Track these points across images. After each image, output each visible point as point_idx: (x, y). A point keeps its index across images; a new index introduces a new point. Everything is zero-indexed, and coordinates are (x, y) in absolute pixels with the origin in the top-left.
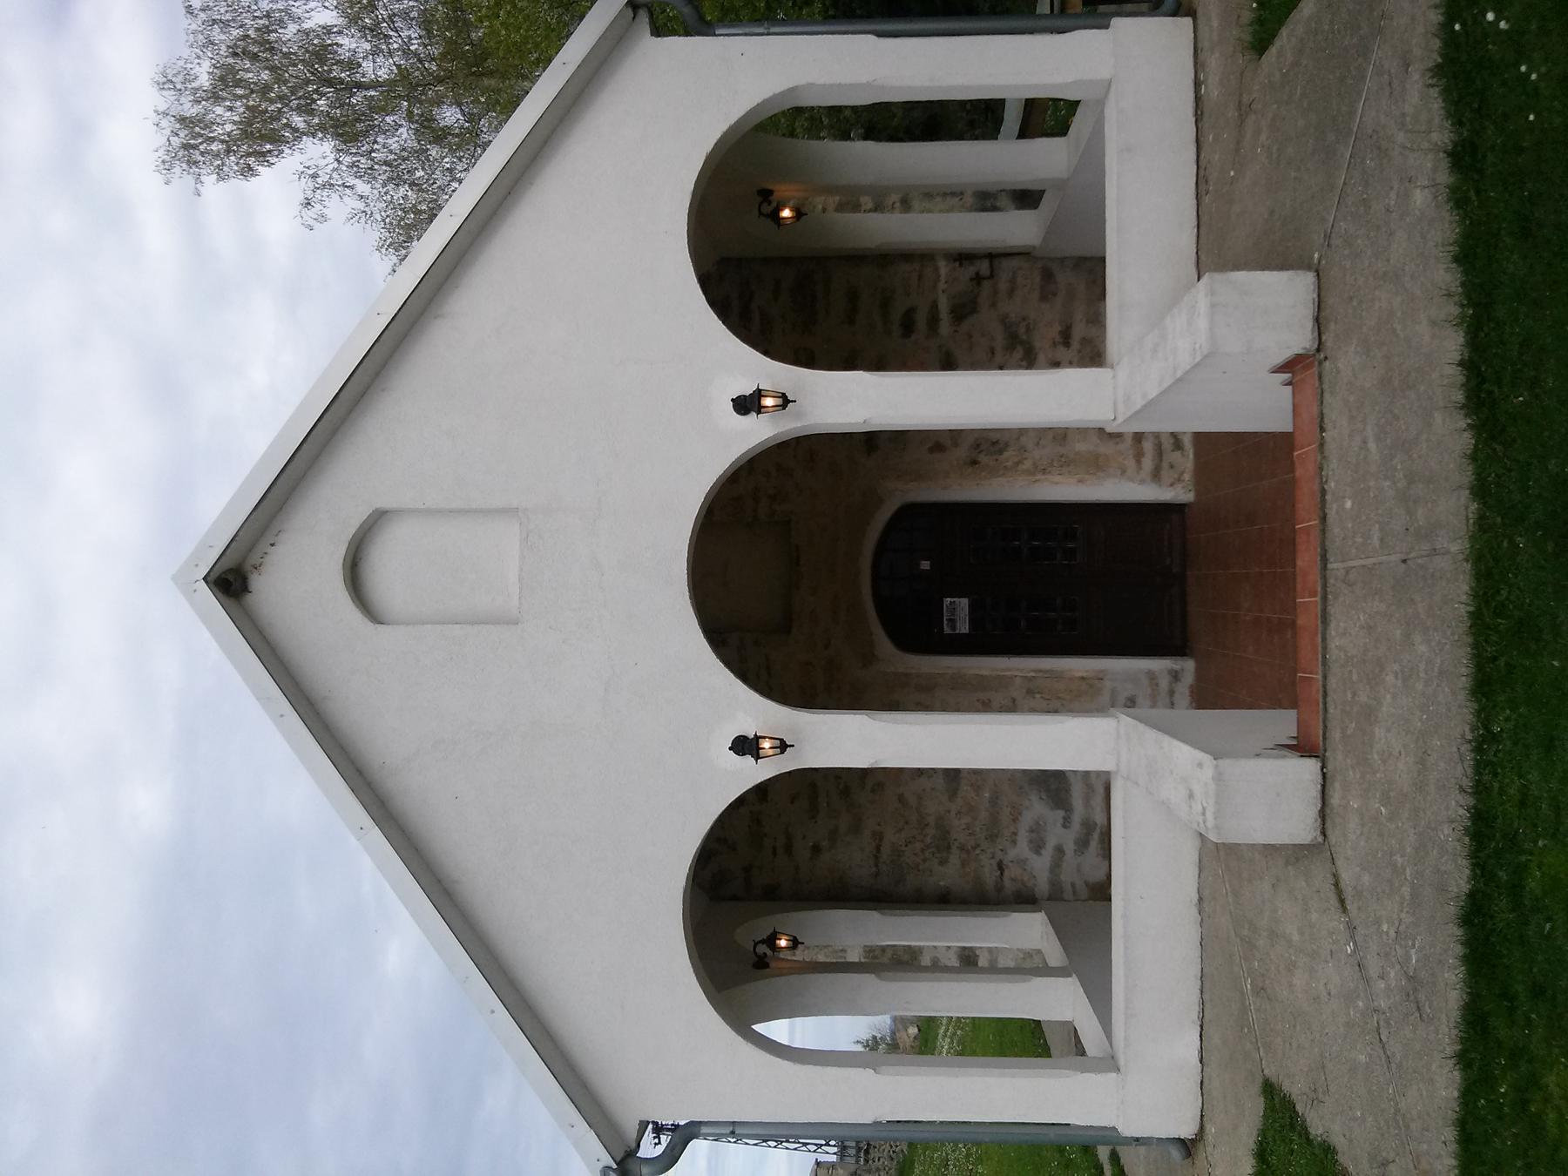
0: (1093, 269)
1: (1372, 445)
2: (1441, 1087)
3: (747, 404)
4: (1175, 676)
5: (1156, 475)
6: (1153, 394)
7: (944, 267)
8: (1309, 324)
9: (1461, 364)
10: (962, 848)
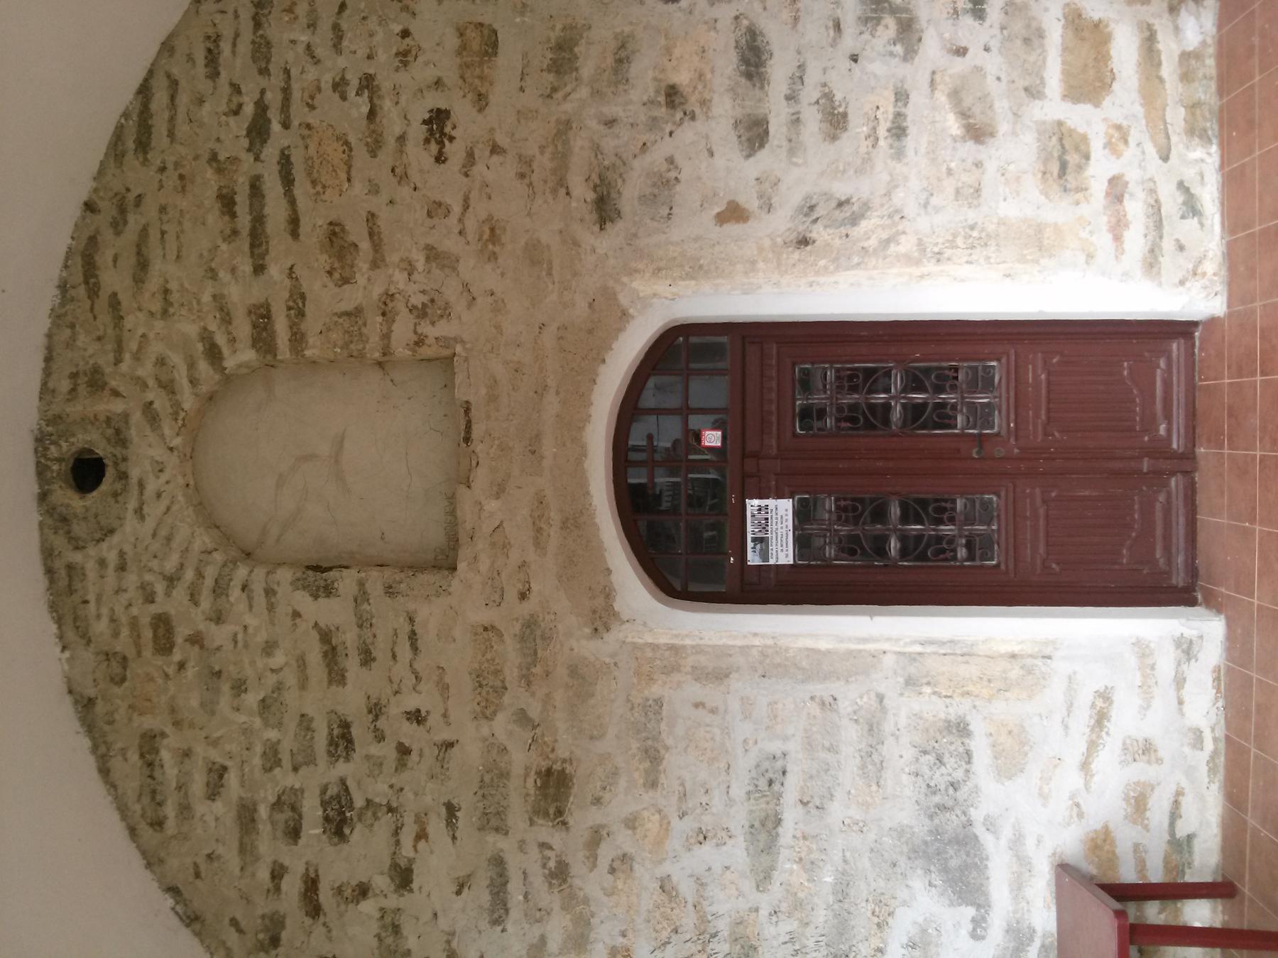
4: (1187, 649)
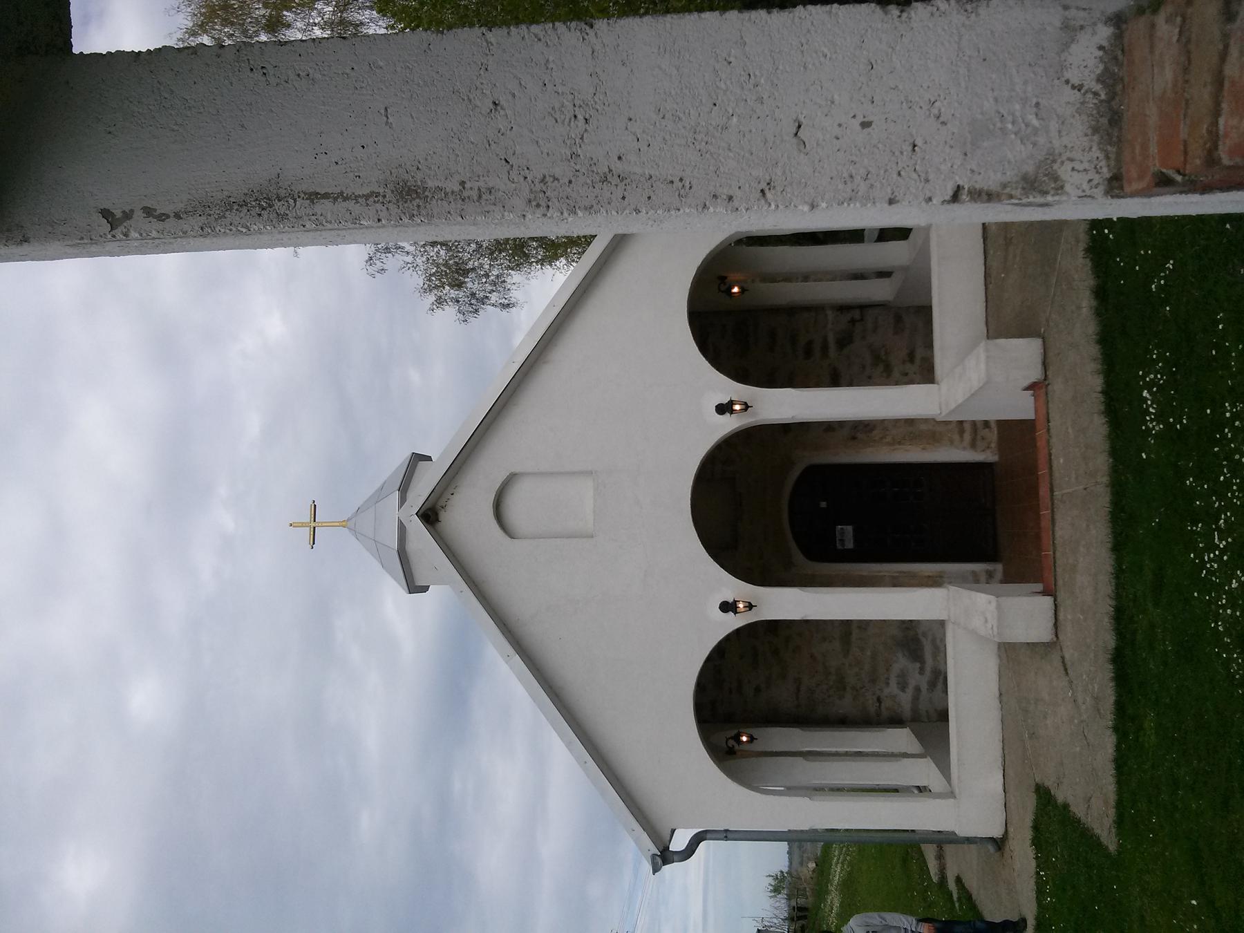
0: (924, 312)
1: (1070, 430)
2: (1109, 742)
3: (723, 409)
5: (973, 445)
6: (960, 401)
7: (829, 312)
8: (1040, 366)
9: (1102, 392)
10: (853, 688)
